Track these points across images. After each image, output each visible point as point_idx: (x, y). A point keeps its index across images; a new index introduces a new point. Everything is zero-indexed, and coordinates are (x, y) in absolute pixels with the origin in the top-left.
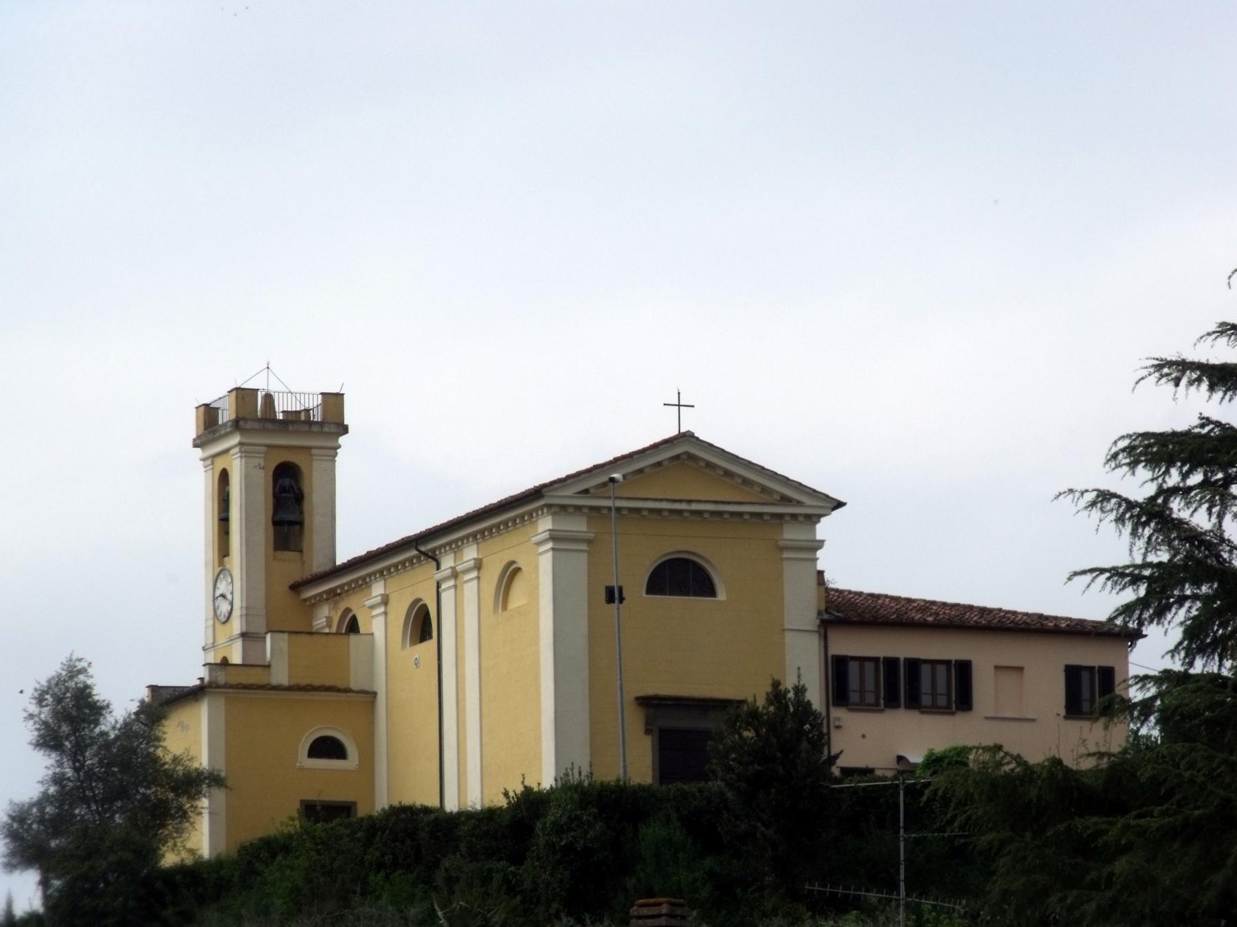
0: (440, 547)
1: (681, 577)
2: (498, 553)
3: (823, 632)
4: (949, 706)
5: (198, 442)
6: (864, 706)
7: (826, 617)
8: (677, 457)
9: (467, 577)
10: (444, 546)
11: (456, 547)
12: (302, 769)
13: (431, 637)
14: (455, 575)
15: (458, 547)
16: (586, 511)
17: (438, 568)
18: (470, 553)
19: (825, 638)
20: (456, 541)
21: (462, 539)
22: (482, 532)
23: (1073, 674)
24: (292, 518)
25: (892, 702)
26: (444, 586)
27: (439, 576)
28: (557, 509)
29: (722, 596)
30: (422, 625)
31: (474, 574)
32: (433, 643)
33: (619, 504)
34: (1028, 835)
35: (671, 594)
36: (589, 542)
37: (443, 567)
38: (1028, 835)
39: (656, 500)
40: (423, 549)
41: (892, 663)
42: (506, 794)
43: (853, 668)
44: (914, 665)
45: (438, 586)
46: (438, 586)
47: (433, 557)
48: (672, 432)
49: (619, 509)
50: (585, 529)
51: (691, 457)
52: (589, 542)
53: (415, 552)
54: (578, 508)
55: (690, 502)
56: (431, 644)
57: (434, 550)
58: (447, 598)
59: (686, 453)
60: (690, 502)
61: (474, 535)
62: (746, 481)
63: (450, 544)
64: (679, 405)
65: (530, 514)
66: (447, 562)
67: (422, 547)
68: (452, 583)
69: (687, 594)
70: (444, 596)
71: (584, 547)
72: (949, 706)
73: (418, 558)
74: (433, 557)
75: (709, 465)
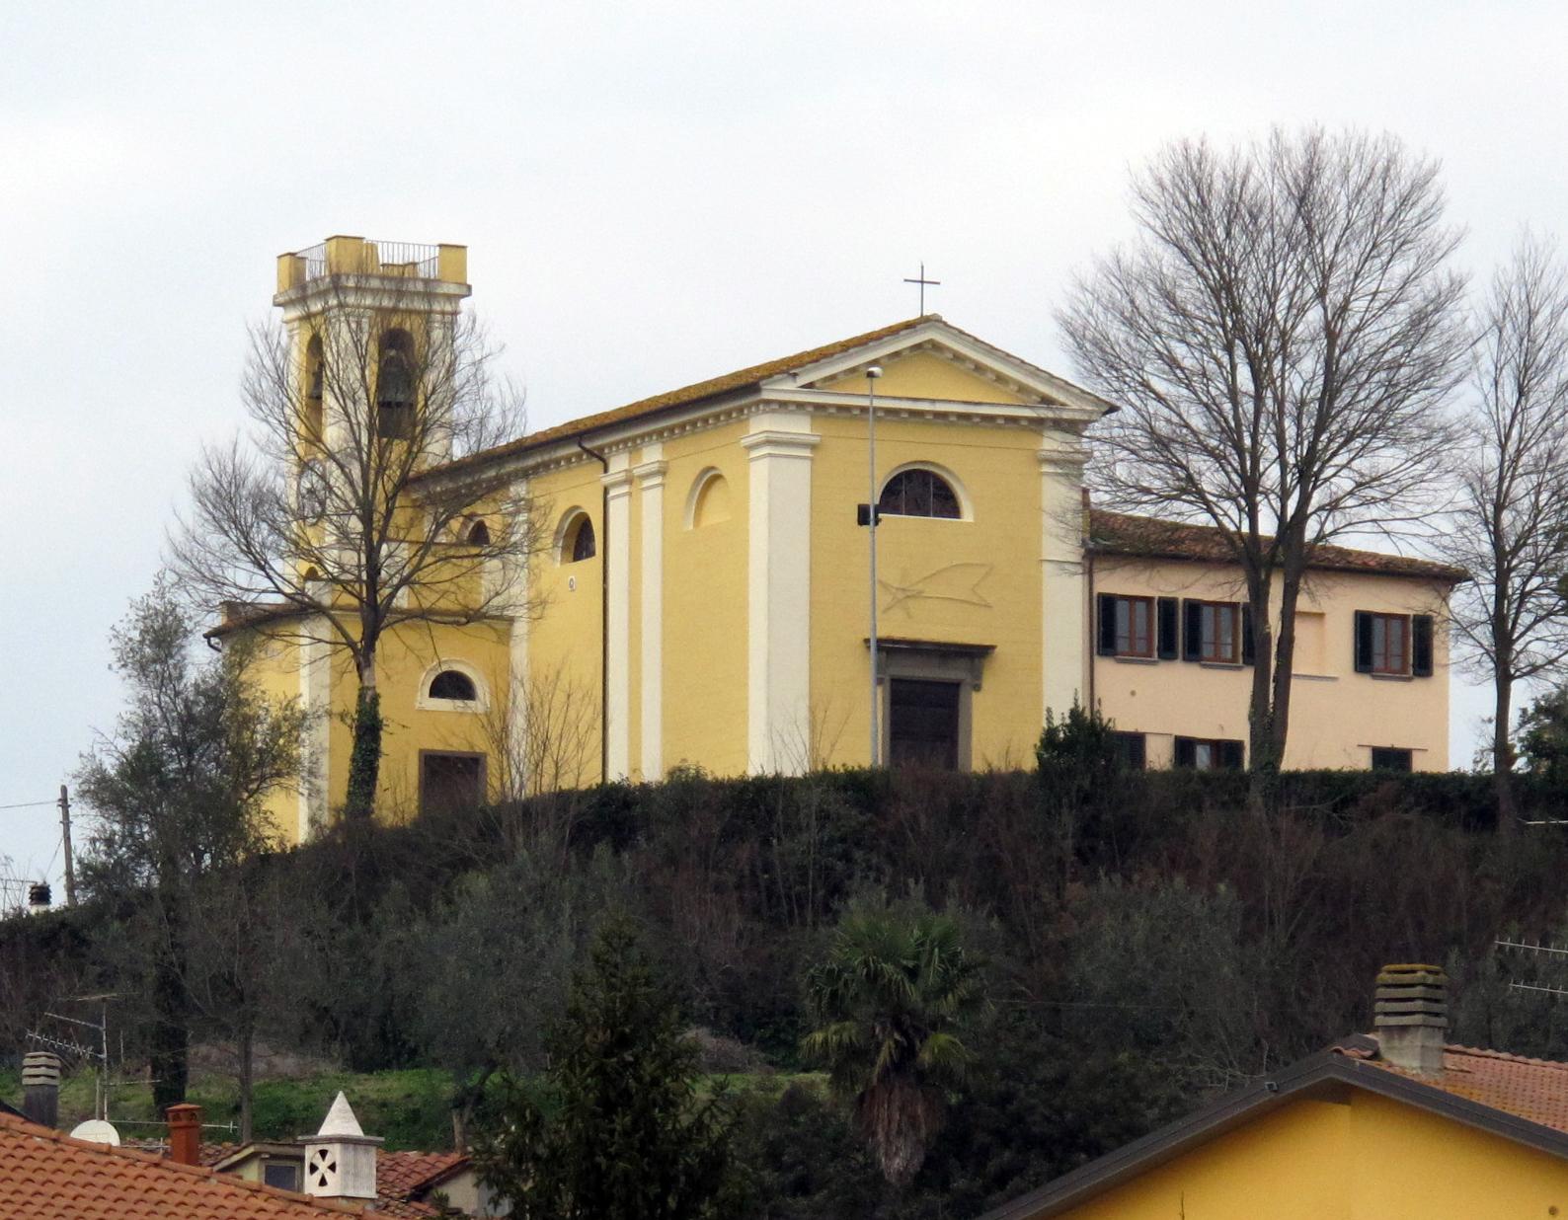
0: (610, 446)
1: (920, 492)
2: (693, 455)
3: (1087, 564)
4: (1234, 659)
5: (281, 299)
6: (1138, 656)
7: (1091, 545)
8: (918, 347)
9: (646, 483)
10: (617, 444)
11: (633, 446)
12: (421, 711)
13: (591, 553)
14: (629, 480)
15: (635, 445)
16: (810, 409)
17: (606, 470)
18: (652, 455)
19: (1090, 574)
20: (633, 439)
21: (642, 437)
22: (671, 430)
23: (1364, 622)
24: (401, 397)
25: (1167, 652)
26: (612, 493)
27: (607, 480)
28: (776, 407)
29: (968, 515)
30: (581, 539)
31: (658, 480)
32: (596, 561)
33: (877, 403)
34: (91, 1048)
35: (936, 515)
36: (813, 447)
37: (612, 469)
38: (91, 1048)
39: (895, 398)
40: (588, 445)
41: (1168, 606)
42: (1110, 720)
43: (1121, 609)
44: (1194, 608)
45: (606, 491)
46: (606, 491)
47: (601, 458)
48: (912, 315)
49: (876, 409)
50: (807, 431)
51: (936, 346)
52: (813, 447)
53: (576, 449)
54: (800, 405)
55: (933, 401)
56: (593, 564)
57: (601, 449)
58: (619, 509)
59: (931, 341)
60: (933, 401)
61: (660, 433)
62: (1000, 378)
63: (625, 441)
64: (922, 282)
65: (740, 410)
66: (619, 464)
67: (589, 439)
68: (625, 489)
69: (926, 514)
70: (612, 504)
71: (807, 453)
72: (1234, 659)
73: (579, 456)
74: (601, 458)
75: (958, 357)
